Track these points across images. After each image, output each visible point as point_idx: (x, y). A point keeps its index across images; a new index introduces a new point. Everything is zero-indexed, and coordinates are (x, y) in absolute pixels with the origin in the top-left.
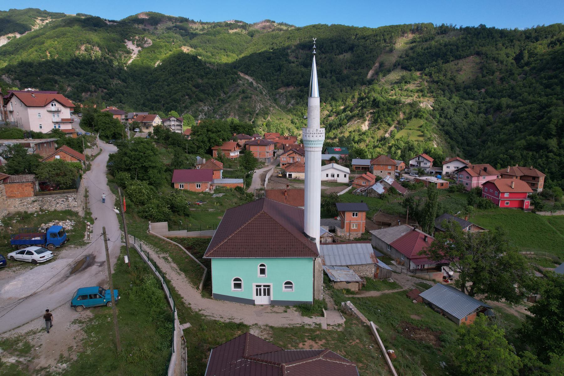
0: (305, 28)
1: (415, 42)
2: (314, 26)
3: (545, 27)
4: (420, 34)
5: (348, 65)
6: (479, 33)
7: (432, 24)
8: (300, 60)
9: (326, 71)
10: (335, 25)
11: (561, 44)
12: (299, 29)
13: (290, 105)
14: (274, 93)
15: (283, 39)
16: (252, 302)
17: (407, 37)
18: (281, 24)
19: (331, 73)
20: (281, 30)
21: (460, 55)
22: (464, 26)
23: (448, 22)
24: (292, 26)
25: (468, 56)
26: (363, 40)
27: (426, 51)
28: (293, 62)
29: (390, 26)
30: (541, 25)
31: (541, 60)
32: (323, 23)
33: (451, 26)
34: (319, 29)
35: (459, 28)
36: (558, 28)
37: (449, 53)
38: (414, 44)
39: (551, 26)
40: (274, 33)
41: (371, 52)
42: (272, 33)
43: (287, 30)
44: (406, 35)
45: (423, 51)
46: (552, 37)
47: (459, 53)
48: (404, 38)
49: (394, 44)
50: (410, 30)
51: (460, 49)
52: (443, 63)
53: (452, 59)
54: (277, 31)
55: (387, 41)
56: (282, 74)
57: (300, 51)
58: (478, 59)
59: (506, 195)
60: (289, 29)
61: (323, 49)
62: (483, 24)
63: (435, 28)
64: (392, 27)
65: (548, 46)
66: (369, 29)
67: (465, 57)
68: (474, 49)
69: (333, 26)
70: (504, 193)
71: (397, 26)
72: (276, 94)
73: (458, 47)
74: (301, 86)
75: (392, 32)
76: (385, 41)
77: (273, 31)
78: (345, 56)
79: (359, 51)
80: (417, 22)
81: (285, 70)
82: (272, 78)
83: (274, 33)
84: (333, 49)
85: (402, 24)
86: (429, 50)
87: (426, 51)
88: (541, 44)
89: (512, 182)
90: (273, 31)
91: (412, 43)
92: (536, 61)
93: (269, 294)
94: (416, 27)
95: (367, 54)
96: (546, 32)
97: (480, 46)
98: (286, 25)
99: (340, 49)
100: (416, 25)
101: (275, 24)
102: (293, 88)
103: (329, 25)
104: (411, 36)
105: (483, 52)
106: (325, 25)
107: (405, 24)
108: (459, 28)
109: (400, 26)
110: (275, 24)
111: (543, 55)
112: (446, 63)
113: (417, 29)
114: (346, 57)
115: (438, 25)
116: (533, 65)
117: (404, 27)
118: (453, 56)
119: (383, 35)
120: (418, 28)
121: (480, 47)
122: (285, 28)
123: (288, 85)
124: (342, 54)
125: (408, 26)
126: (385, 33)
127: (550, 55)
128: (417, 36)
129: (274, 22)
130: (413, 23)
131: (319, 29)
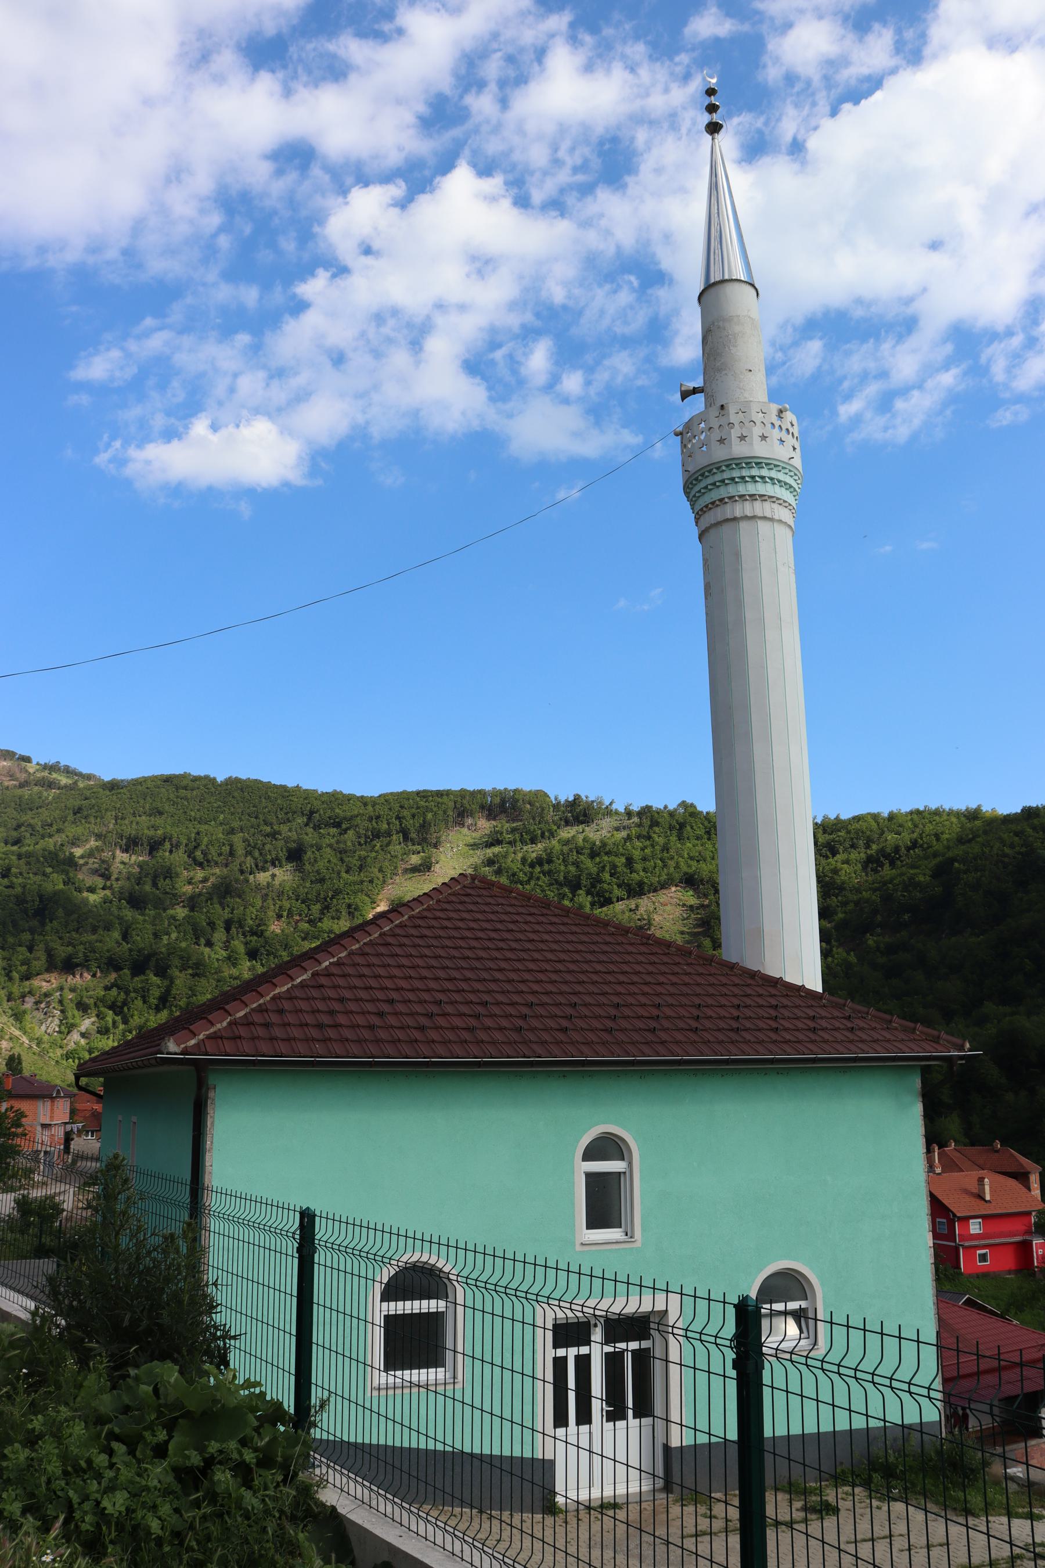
0: (137, 782)
1: (498, 842)
2: (168, 780)
3: (844, 821)
4: (514, 821)
5: (287, 904)
6: (682, 826)
7: (546, 795)
8: (116, 886)
9: (212, 925)
10: (237, 780)
11: (892, 864)
12: (114, 786)
13: (75, 1036)
14: (16, 990)
15: (57, 813)
16: (526, 1485)
17: (473, 828)
18: (53, 768)
19: (228, 929)
20: (51, 785)
21: (641, 884)
22: (636, 808)
23: (590, 793)
24: (89, 777)
25: (664, 886)
26: (333, 831)
27: (538, 869)
28: (92, 890)
29: (418, 793)
30: (832, 817)
31: (857, 903)
32: (197, 771)
33: (601, 803)
34: (185, 788)
35: (622, 810)
36: (874, 824)
37: (606, 876)
38: (497, 849)
39: (857, 819)
40: (26, 792)
41: (361, 868)
42: (19, 792)
43: (73, 787)
44: (470, 821)
45: (527, 869)
46: (868, 846)
47: (634, 875)
48: (465, 830)
49: (436, 846)
50: (482, 807)
51: (638, 866)
52: (593, 904)
53: (617, 892)
54: (36, 789)
55: (413, 835)
56: (48, 928)
57: (118, 852)
58: (690, 898)
59: (975, 1227)
60: (81, 785)
61: (198, 853)
62: (689, 801)
63: (557, 806)
64: (423, 795)
65: (865, 868)
66: (350, 798)
67: (655, 891)
68: (677, 867)
69: (233, 784)
70: (967, 1219)
71: (439, 794)
72: (23, 996)
73: (630, 862)
74: (118, 969)
75: (428, 809)
76: (406, 838)
77: (21, 786)
78: (273, 876)
79: (321, 865)
80: (501, 787)
81: (60, 912)
82: (11, 940)
83: (26, 792)
84: (232, 853)
85: (456, 787)
86: (546, 867)
87: (538, 869)
88: (847, 862)
89: (981, 1180)
90: (21, 786)
91: (489, 845)
92: (845, 904)
93: (643, 1409)
94: (497, 800)
95: (347, 872)
96: (849, 832)
97: (691, 858)
98: (68, 771)
99: (257, 854)
100: (495, 793)
101: (31, 768)
102: (87, 976)
103: (220, 779)
104: (485, 826)
105: (705, 875)
106: (207, 777)
107: (462, 790)
108: (622, 810)
109: (448, 793)
110: (31, 768)
111: (858, 891)
112: (602, 906)
113: (504, 806)
114: (277, 882)
115: (562, 799)
116: (841, 915)
117: (463, 797)
118: (619, 886)
119: (398, 818)
120: (503, 801)
121: (694, 863)
122: (64, 780)
123: (69, 967)
124: (264, 869)
125: (473, 794)
126: (405, 813)
127: (875, 890)
128: (504, 825)
129: (28, 760)
130: (488, 788)
131: (185, 788)
